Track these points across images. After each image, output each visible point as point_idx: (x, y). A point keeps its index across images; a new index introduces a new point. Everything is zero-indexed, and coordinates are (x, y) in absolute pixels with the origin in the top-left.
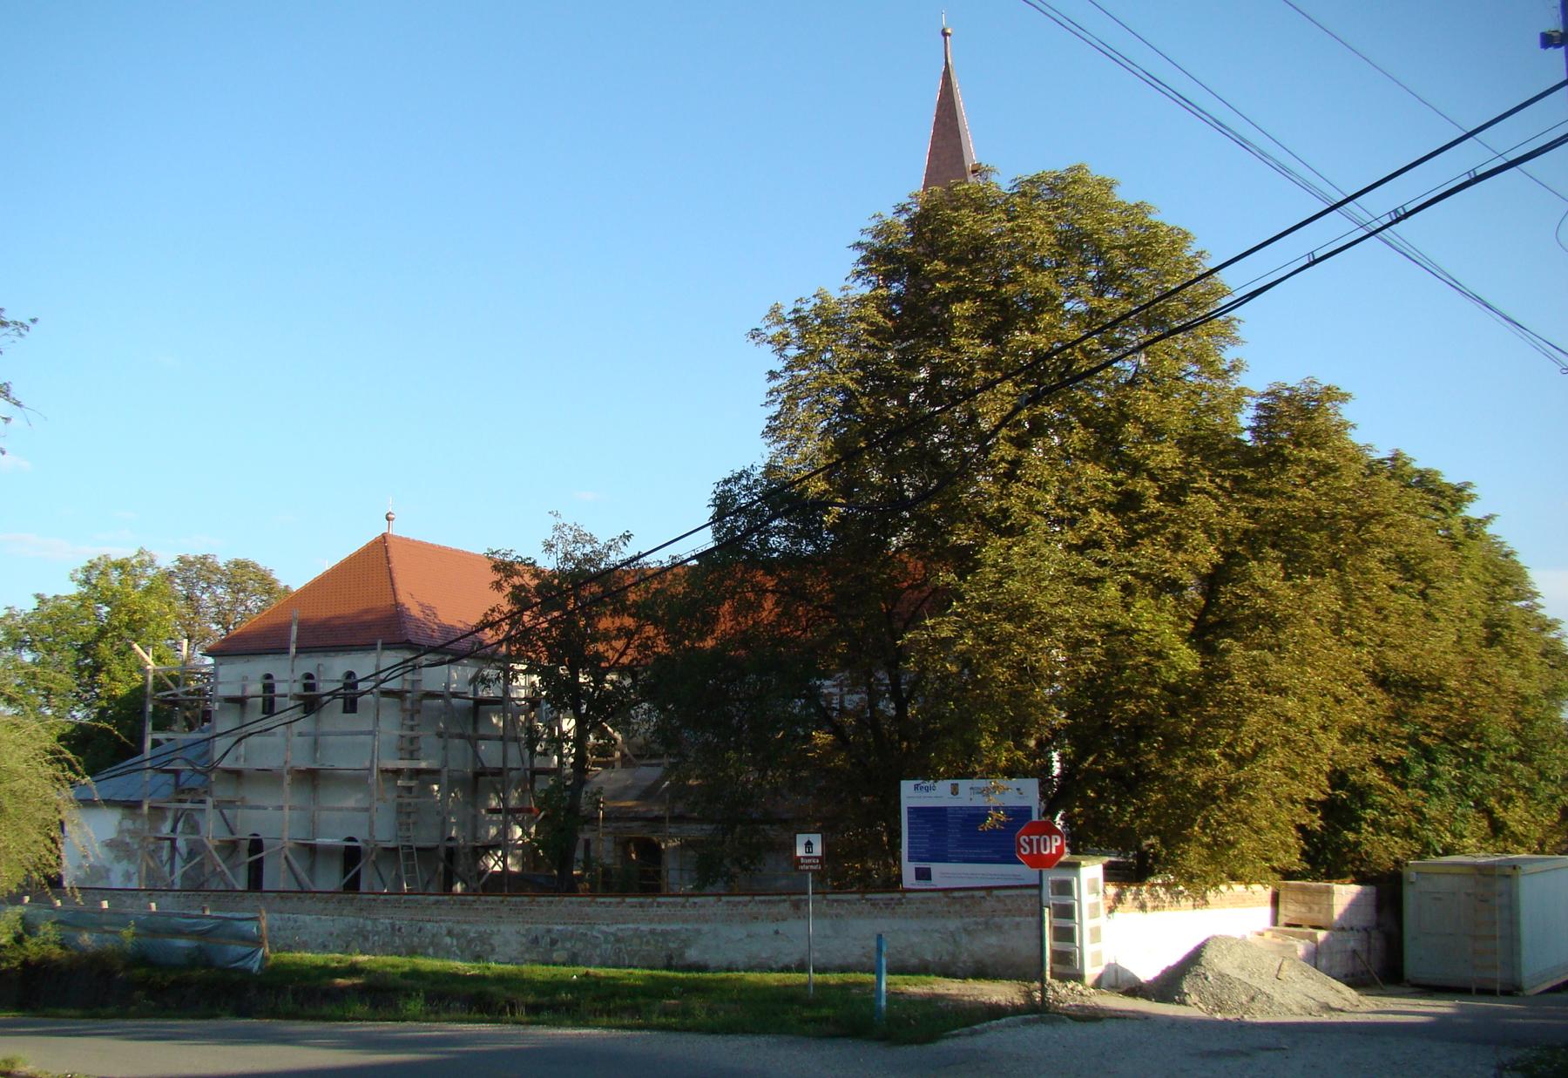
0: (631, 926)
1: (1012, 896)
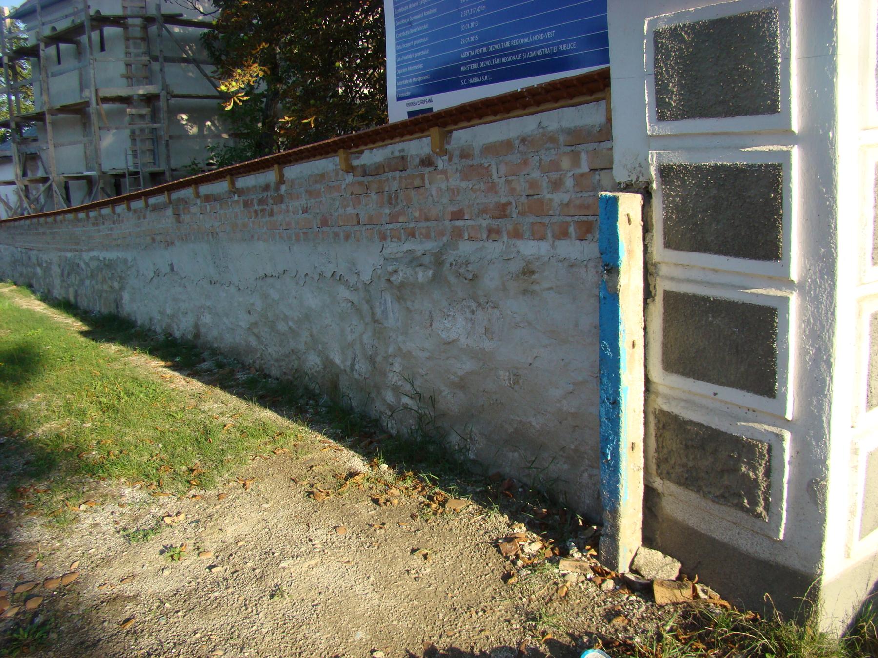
1: (508, 145)
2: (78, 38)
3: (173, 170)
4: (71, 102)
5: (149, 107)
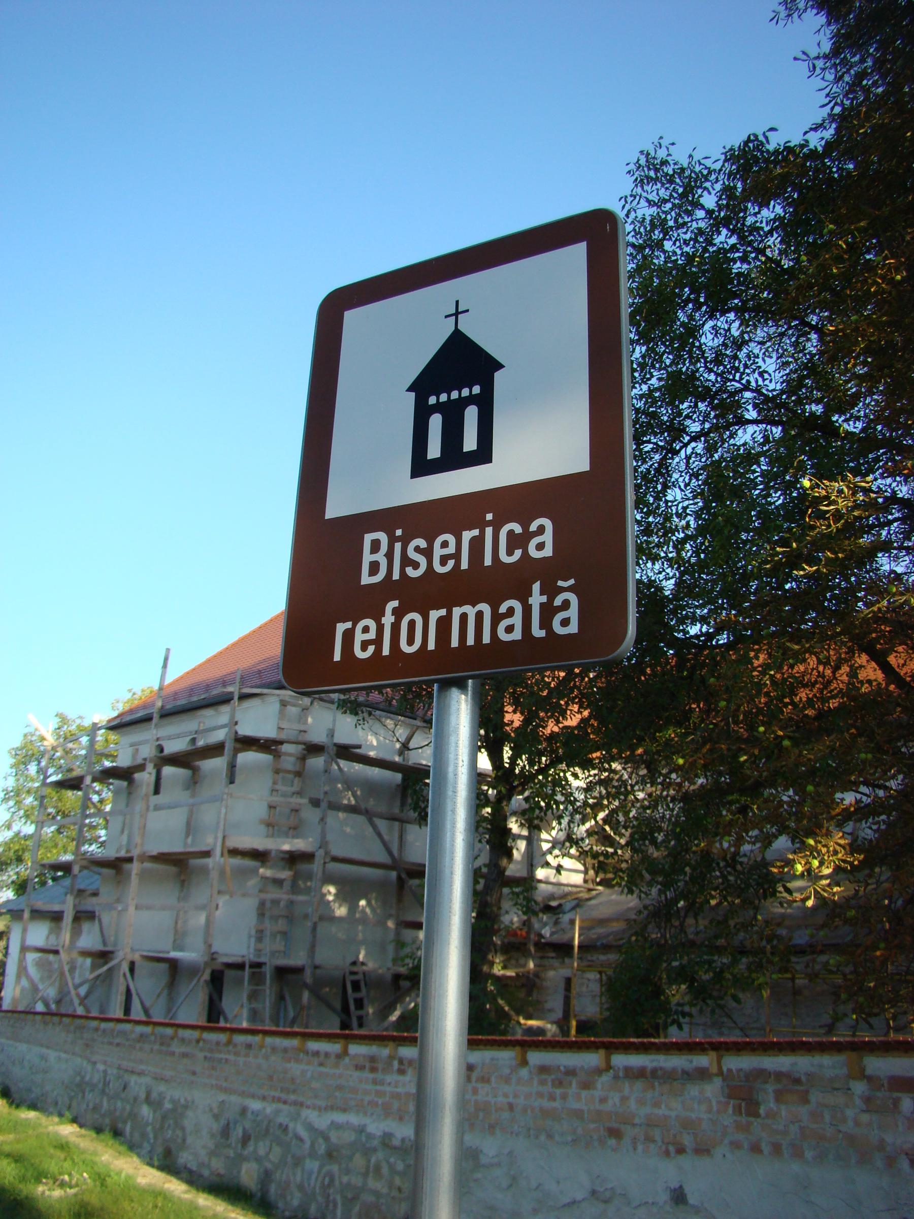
0: (354, 1119)
2: (197, 763)
3: (316, 967)
4: (165, 849)
5: (290, 869)
